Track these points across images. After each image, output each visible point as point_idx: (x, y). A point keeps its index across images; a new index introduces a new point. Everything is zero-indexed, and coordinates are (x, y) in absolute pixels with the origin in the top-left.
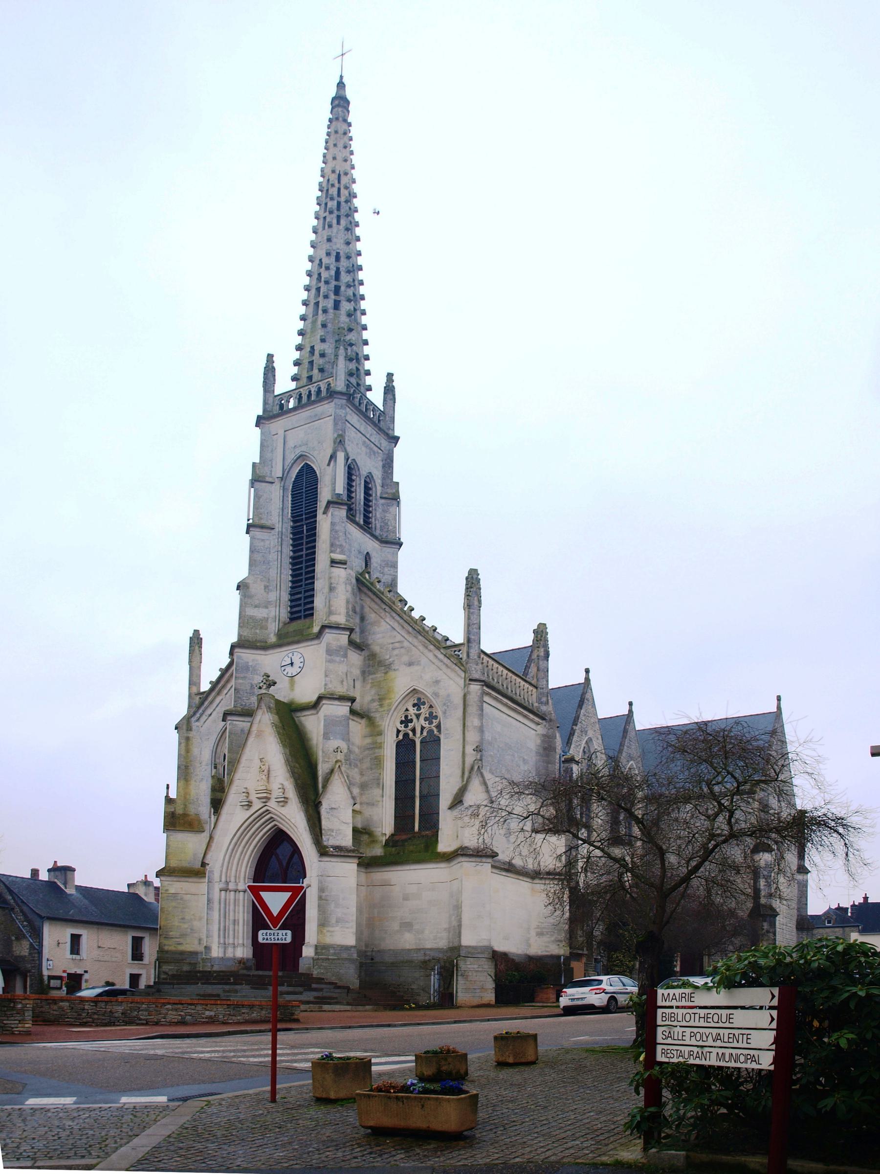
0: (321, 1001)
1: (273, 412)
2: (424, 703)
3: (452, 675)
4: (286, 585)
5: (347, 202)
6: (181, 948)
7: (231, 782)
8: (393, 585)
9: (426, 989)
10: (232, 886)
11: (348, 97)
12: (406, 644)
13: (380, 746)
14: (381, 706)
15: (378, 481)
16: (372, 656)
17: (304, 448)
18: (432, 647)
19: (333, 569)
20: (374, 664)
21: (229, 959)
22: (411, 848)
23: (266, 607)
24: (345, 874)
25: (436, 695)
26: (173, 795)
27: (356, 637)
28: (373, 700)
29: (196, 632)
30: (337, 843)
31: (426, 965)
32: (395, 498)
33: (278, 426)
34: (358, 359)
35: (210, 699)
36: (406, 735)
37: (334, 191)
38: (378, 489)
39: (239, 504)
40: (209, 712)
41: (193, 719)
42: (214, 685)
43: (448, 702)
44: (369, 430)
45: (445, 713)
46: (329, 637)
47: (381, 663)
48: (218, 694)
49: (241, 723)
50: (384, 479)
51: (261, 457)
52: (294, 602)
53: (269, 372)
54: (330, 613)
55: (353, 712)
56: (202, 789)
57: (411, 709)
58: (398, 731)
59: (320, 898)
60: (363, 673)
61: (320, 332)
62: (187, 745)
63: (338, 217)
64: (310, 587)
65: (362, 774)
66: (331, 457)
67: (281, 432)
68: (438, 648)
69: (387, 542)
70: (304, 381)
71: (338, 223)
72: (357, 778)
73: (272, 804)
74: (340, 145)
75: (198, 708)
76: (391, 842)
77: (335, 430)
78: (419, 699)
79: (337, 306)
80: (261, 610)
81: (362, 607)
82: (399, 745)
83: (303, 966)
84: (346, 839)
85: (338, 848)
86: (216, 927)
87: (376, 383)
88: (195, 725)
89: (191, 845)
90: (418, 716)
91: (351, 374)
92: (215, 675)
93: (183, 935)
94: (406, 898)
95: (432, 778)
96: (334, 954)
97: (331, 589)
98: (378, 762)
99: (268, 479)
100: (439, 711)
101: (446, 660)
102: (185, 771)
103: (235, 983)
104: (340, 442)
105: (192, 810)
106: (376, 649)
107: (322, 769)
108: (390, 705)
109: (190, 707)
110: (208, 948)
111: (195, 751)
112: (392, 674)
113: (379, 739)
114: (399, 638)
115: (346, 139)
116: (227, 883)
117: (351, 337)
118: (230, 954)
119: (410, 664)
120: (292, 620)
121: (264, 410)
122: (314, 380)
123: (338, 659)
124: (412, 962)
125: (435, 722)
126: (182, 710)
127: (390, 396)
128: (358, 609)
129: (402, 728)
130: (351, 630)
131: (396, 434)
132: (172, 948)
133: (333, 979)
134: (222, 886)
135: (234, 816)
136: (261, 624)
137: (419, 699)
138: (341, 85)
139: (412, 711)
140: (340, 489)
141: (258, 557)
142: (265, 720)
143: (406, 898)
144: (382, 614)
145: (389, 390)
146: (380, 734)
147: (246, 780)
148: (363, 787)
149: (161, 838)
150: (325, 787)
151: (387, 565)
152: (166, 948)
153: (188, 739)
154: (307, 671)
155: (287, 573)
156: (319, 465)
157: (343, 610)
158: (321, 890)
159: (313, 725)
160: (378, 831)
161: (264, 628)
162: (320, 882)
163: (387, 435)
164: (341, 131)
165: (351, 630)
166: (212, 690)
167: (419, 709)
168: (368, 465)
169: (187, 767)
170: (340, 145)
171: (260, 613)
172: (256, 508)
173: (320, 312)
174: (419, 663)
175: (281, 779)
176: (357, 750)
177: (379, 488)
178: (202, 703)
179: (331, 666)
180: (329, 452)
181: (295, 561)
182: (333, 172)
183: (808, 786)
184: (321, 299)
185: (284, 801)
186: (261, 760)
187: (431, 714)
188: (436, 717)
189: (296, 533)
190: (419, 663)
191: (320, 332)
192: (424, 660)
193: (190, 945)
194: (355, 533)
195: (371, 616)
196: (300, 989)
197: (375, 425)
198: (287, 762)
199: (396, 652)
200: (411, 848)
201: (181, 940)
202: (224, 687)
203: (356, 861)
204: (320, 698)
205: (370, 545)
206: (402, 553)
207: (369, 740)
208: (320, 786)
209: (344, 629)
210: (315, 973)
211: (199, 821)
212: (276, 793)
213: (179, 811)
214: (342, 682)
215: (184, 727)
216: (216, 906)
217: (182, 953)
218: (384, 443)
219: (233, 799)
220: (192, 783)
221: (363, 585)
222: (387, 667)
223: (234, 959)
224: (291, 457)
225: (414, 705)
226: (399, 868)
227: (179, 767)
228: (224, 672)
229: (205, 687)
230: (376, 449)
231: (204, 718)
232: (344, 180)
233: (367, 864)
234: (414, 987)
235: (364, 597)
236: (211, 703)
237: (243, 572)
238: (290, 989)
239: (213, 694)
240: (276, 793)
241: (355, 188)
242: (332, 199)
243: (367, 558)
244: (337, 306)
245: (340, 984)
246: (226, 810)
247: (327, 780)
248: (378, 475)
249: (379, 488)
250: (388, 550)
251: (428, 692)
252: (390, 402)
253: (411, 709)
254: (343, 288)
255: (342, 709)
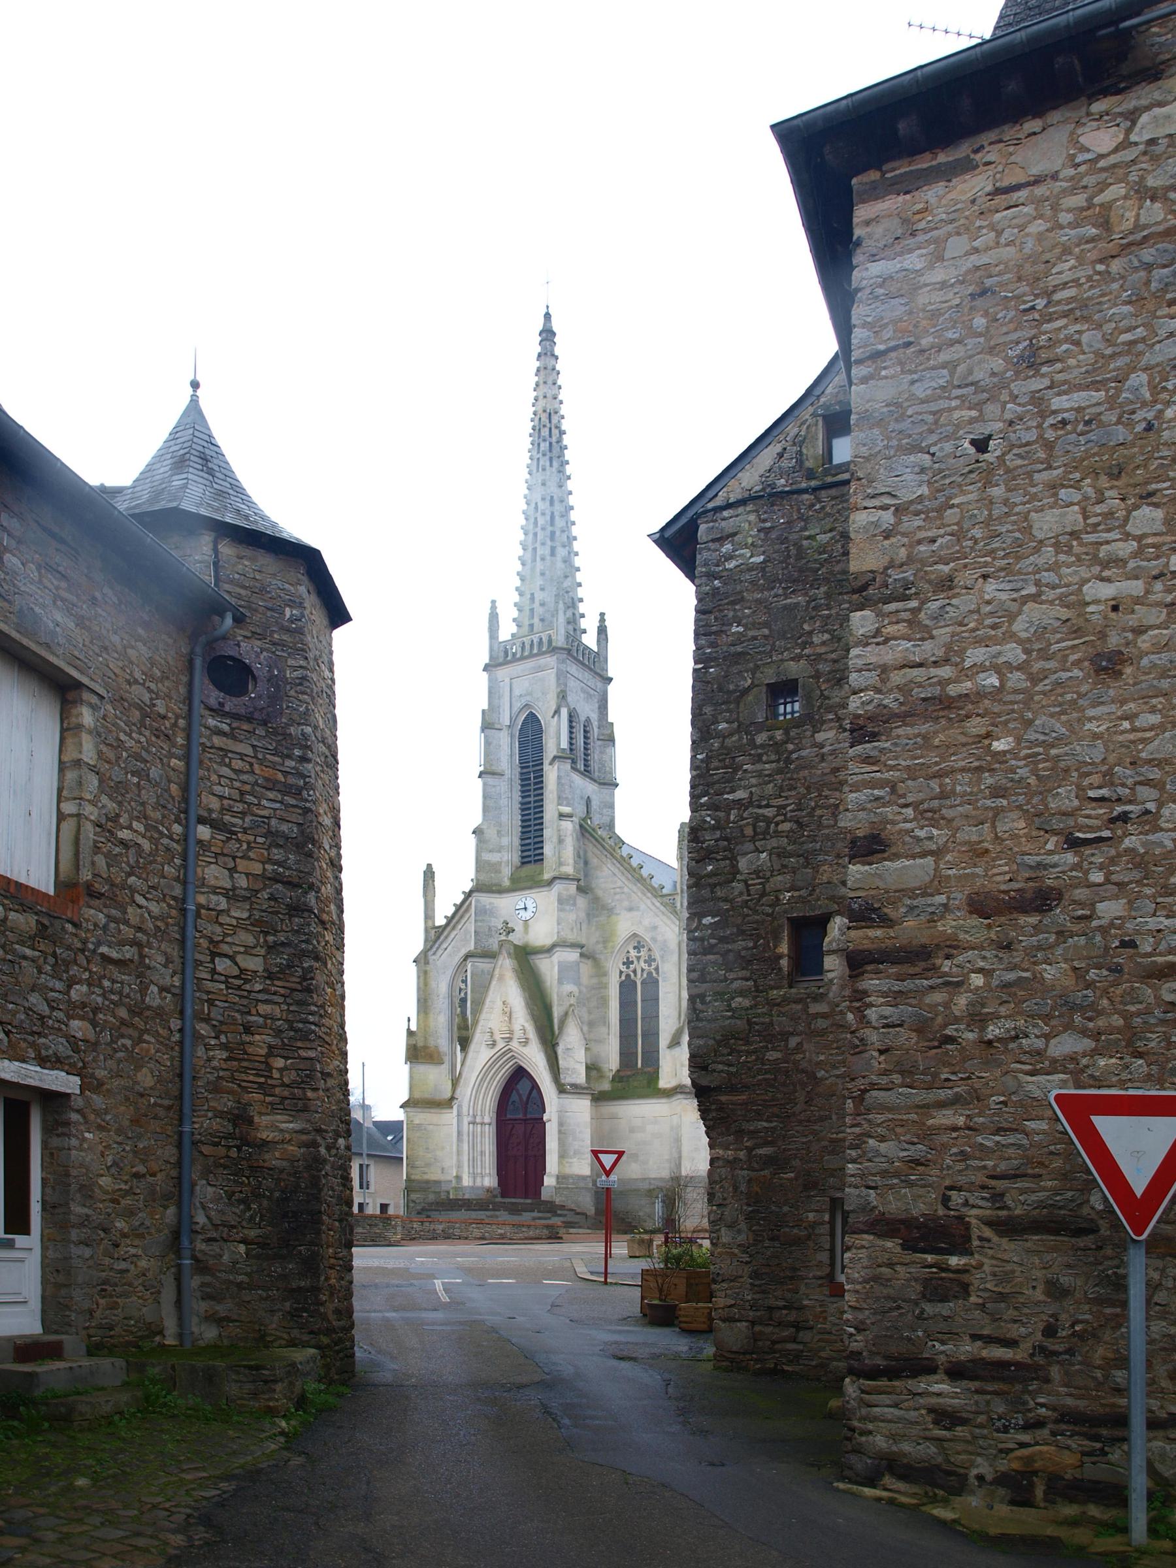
0: (569, 1225)
1: (500, 659)
2: (643, 947)
3: (668, 922)
4: (518, 830)
5: (558, 442)
6: (426, 1177)
7: (476, 1022)
8: (611, 826)
9: (651, 1216)
10: (478, 1120)
11: (554, 329)
12: (626, 890)
13: (605, 986)
14: (605, 948)
15: (595, 724)
16: (596, 900)
17: (528, 698)
18: (649, 895)
19: (563, 823)
20: (598, 909)
21: (478, 1188)
22: (635, 1084)
23: (499, 851)
24: (581, 1109)
25: (654, 939)
26: (414, 1028)
27: (582, 883)
28: (598, 942)
29: (429, 866)
30: (573, 1081)
31: (650, 1193)
32: (611, 740)
33: (503, 673)
34: (573, 603)
35: (445, 933)
36: (628, 976)
37: (545, 432)
38: (595, 731)
39: (470, 751)
40: (444, 946)
41: (430, 953)
42: (450, 920)
43: (664, 948)
44: (586, 676)
45: (662, 957)
46: (558, 887)
47: (604, 907)
48: (454, 928)
49: (483, 965)
50: (600, 720)
51: (490, 704)
52: (525, 848)
53: (494, 618)
54: (560, 864)
55: (582, 955)
56: (441, 1021)
57: (632, 951)
58: (621, 972)
59: (560, 1132)
60: (588, 915)
61: (539, 582)
62: (425, 979)
63: (551, 459)
64: (539, 833)
65: (590, 1013)
66: (556, 712)
67: (507, 680)
68: (655, 897)
69: (604, 784)
70: (526, 629)
71: (551, 465)
72: (586, 1017)
73: (515, 1044)
74: (550, 382)
75: (435, 942)
76: (618, 1078)
77: (558, 684)
78: (639, 942)
79: (553, 553)
80: (495, 854)
81: (585, 852)
82: (622, 984)
83: (545, 1195)
84: (580, 1077)
85: (574, 1086)
86: (465, 1158)
87: (590, 624)
88: (431, 958)
89: (436, 1078)
90: (638, 958)
91: (569, 623)
92: (450, 911)
93: (428, 1165)
94: (632, 1130)
95: (652, 1017)
96: (573, 1183)
97: (561, 841)
98: (604, 1002)
99: (497, 726)
100: (657, 954)
101: (662, 908)
102: (424, 1003)
103: (494, 1210)
104: (562, 696)
105: (431, 1043)
106: (600, 893)
107: (557, 1013)
108: (613, 947)
109: (426, 940)
110: (458, 1178)
111: (433, 984)
112: (614, 918)
113: (604, 980)
114: (619, 884)
115: (555, 373)
116: (474, 1116)
117: (567, 583)
118: (478, 1183)
119: (630, 909)
120: (523, 863)
121: (491, 658)
122: (535, 630)
123: (568, 908)
124: (639, 1190)
125: (654, 965)
126: (418, 945)
127: (603, 636)
128: (582, 853)
129: (624, 968)
130: (579, 880)
131: (610, 675)
132: (418, 1177)
133: (573, 1206)
134: (470, 1119)
135: (480, 1055)
136: (495, 868)
137: (639, 942)
138: (547, 316)
139: (633, 953)
140: (564, 744)
141: (491, 803)
142: (506, 965)
143: (632, 1130)
144: (604, 859)
145: (602, 630)
146: (605, 974)
147: (491, 1020)
148: (591, 1024)
149: (403, 1070)
150: (561, 1028)
151: (605, 806)
152: (413, 1177)
153: (426, 972)
154: (538, 915)
155: (517, 821)
156: (544, 714)
157: (571, 861)
158: (561, 1124)
159: (549, 968)
160: (605, 1067)
161: (498, 871)
162: (559, 1117)
163: (601, 676)
164: (550, 367)
165: (579, 880)
166: (447, 925)
167: (639, 952)
168: (587, 710)
169: (426, 1000)
170: (550, 382)
171: (494, 858)
172: (487, 755)
173: (538, 559)
174: (638, 909)
175: (522, 1020)
176: (584, 990)
177: (596, 730)
178: (439, 938)
179: (562, 915)
180: (554, 708)
181: (524, 807)
182: (545, 411)
183: (721, 1152)
184: (538, 545)
185: (526, 1042)
186: (504, 1003)
187: (650, 956)
188: (654, 960)
189: (524, 779)
190: (638, 909)
191: (539, 582)
192: (642, 907)
193: (434, 1175)
194: (578, 779)
195: (594, 861)
196: (549, 1215)
197: (591, 669)
198: (528, 1005)
199: (617, 897)
200: (635, 1084)
201: (426, 1170)
202: (458, 922)
203: (590, 1097)
204: (554, 946)
205: (590, 788)
206: (617, 791)
207: (594, 981)
208: (556, 1027)
209: (573, 879)
210: (558, 1201)
211: (439, 1053)
212: (518, 1034)
213: (420, 1044)
214: (572, 929)
215: (422, 960)
216: (465, 1138)
217: (427, 1182)
218: (599, 685)
219: (479, 1039)
220: (431, 1015)
221: (585, 831)
222: (610, 911)
223: (482, 1187)
224: (518, 705)
225: (635, 948)
226: (625, 1102)
227: (419, 1000)
228: (458, 908)
229: (440, 921)
230: (592, 692)
231: (440, 952)
232: (555, 419)
233: (599, 1098)
234: (641, 1214)
235: (586, 842)
236: (446, 937)
237: (477, 819)
238: (540, 1215)
239: (449, 929)
240: (518, 1034)
241: (565, 426)
242: (544, 440)
243: (588, 801)
244: (553, 553)
245: (579, 1210)
246: (473, 1047)
247: (562, 1022)
248: (594, 717)
249: (596, 730)
250: (606, 791)
251: (647, 937)
252: (603, 645)
253: (632, 951)
254: (558, 533)
255: (572, 956)
